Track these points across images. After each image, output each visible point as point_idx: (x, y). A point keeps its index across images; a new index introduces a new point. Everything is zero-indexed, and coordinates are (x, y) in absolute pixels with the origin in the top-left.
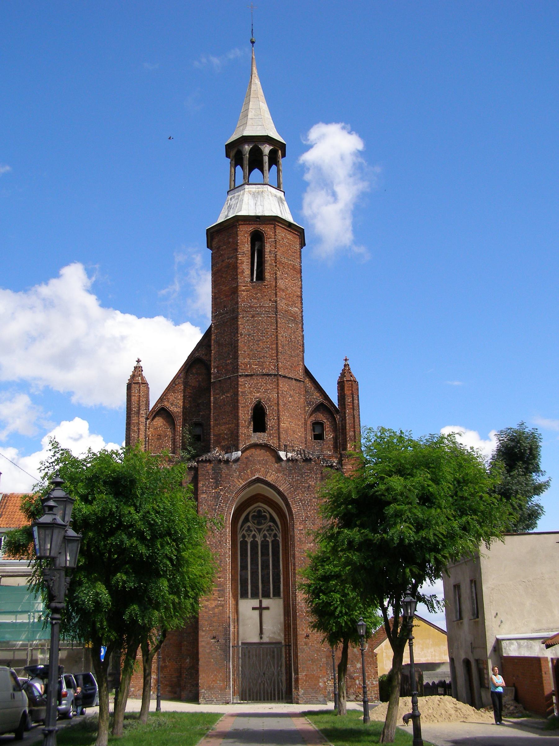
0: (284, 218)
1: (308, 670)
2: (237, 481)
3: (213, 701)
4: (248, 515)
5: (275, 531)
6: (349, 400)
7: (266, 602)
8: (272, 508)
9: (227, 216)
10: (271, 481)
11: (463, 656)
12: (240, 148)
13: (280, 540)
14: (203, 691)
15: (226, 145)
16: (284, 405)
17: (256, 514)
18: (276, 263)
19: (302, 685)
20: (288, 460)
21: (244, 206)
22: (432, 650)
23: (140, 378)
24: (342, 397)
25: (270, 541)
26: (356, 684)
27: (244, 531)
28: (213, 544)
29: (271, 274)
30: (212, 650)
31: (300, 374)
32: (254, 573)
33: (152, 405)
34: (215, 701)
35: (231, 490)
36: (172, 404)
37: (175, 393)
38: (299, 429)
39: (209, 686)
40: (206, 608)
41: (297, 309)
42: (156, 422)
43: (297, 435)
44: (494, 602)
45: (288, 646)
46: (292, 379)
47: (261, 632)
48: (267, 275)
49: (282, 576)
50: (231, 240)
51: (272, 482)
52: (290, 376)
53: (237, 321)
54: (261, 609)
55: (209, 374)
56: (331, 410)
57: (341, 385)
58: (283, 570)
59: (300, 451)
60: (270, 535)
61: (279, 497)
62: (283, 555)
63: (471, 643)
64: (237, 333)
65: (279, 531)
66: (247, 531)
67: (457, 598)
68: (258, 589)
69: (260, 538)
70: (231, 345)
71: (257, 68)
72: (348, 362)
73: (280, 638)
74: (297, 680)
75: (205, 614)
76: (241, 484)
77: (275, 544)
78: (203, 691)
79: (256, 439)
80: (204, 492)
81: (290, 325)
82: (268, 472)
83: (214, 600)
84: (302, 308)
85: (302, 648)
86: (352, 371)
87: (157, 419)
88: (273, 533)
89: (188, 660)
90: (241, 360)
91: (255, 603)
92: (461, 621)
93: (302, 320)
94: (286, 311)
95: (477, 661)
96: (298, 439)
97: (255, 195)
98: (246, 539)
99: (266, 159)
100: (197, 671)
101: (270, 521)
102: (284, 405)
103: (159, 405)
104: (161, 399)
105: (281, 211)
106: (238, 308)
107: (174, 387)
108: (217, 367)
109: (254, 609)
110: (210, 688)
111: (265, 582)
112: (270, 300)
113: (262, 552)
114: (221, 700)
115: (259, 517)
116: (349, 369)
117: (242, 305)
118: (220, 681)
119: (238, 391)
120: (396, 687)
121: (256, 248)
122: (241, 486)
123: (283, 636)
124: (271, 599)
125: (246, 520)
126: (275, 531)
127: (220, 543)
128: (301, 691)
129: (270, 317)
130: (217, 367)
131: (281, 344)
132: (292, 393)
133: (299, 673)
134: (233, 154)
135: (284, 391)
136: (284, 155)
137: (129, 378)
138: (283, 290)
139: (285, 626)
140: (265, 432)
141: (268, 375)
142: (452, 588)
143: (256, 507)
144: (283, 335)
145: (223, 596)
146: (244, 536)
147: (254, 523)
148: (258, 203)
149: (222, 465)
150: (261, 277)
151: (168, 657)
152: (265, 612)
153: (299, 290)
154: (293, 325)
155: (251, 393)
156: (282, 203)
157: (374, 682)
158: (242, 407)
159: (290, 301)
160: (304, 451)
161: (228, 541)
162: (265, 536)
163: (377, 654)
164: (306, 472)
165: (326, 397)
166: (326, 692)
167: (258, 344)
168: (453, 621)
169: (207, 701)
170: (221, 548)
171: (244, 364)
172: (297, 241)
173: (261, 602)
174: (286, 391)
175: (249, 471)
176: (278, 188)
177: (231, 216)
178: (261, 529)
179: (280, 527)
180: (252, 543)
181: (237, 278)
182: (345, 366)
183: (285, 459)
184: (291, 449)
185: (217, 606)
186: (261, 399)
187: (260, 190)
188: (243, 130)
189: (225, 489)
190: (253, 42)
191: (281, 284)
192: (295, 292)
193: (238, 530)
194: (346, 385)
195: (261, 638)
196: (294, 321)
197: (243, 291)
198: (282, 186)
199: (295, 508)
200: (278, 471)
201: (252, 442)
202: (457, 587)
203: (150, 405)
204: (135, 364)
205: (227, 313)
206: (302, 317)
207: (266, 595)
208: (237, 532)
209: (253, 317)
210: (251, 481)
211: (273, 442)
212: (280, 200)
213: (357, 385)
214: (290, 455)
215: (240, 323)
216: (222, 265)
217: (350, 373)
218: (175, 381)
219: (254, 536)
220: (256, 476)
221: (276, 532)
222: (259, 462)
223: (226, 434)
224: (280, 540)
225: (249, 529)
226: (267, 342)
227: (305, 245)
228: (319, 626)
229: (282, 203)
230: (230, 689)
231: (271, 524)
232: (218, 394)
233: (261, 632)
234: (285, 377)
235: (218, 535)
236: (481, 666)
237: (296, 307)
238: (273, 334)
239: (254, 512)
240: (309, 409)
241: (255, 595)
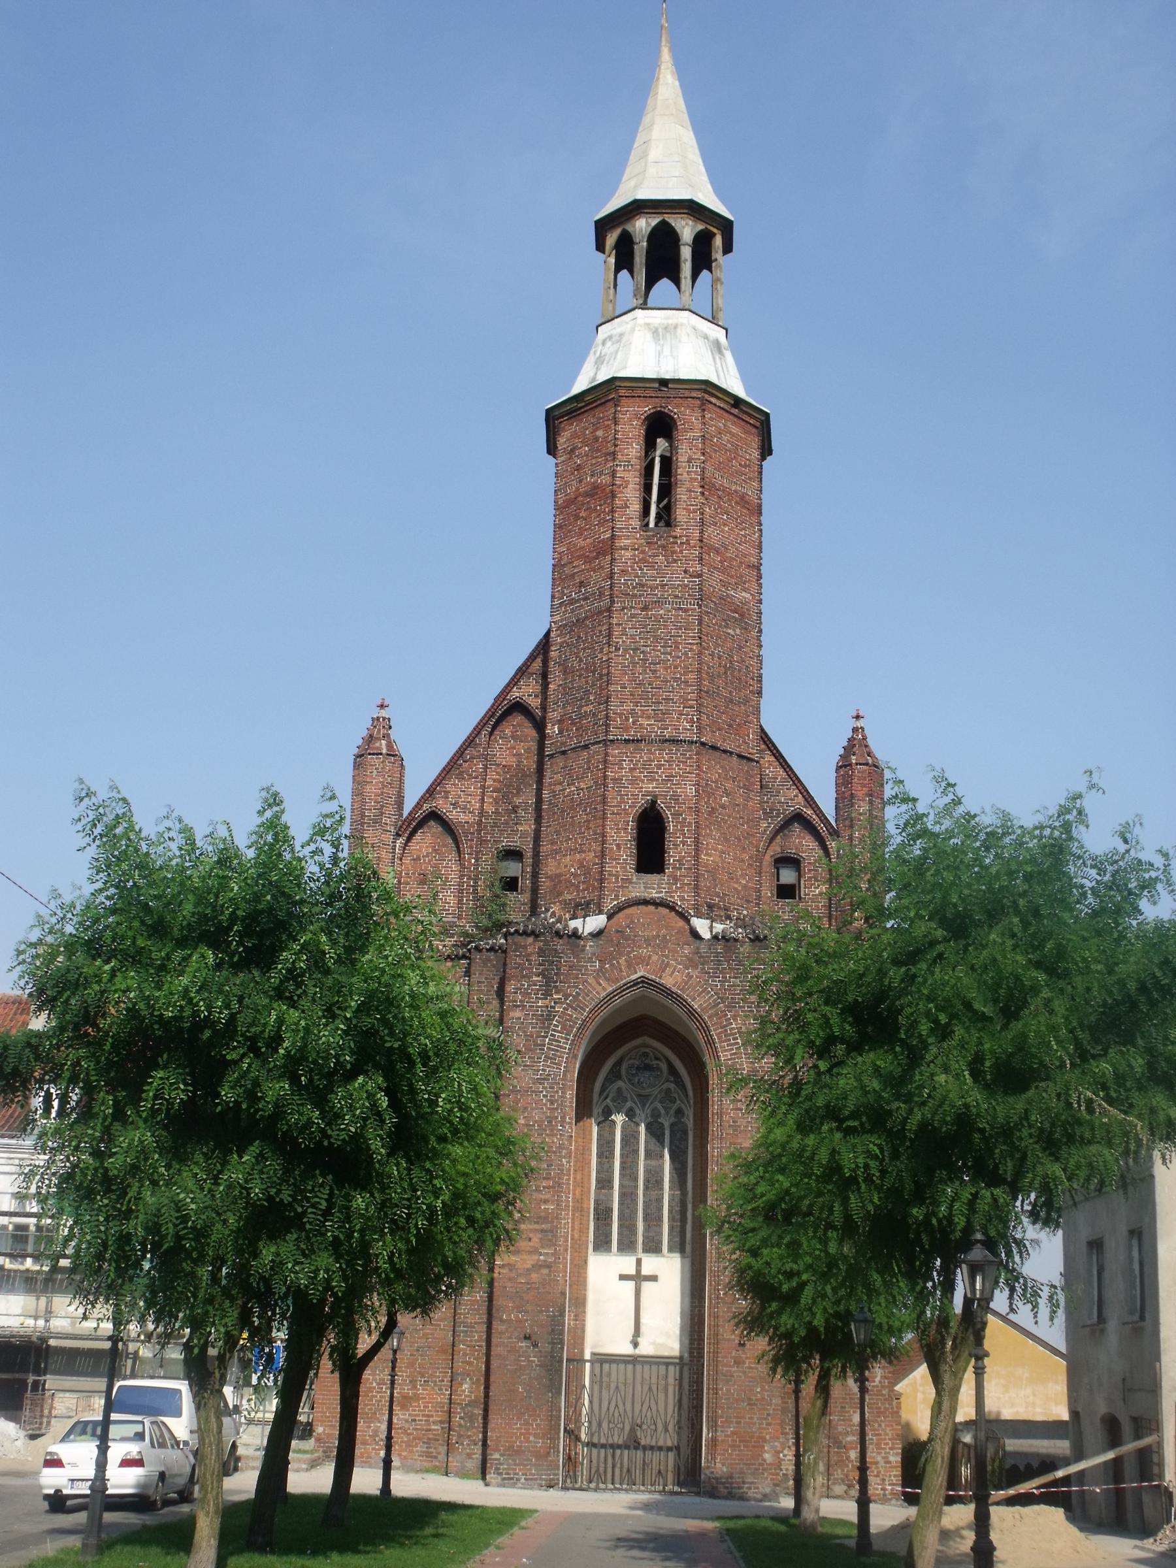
0: (724, 386)
1: (738, 1423)
2: (594, 983)
4: (619, 1063)
7: (651, 1264)
8: (673, 1051)
9: (594, 379)
10: (674, 986)
11: (1102, 1409)
12: (629, 228)
14: (496, 1456)
15: (596, 222)
18: (702, 487)
19: (723, 1455)
20: (715, 937)
22: (1029, 1391)
23: (383, 742)
24: (844, 800)
25: (667, 1124)
26: (848, 1458)
27: (608, 1100)
28: (534, 1125)
29: (689, 511)
30: (521, 1366)
31: (752, 746)
32: (628, 1196)
33: (408, 807)
34: (523, 1480)
35: (581, 1001)
36: (455, 805)
37: (464, 778)
38: (742, 869)
39: (511, 1447)
40: (511, 1270)
41: (747, 595)
42: (417, 843)
43: (737, 882)
46: (731, 753)
48: (680, 514)
50: (600, 433)
51: (674, 989)
54: (638, 1278)
55: (542, 736)
56: (818, 831)
57: (844, 766)
58: (693, 1193)
62: (694, 1157)
63: (1124, 1379)
65: (689, 1102)
67: (1095, 1272)
69: (643, 1116)
70: (593, 672)
71: (672, 50)
74: (714, 1442)
75: (509, 1285)
76: (604, 989)
78: (496, 1456)
79: (642, 889)
80: (519, 1006)
81: (730, 631)
82: (668, 965)
83: (530, 1253)
85: (727, 1371)
86: (870, 741)
87: (418, 836)
88: (675, 1107)
89: (465, 1386)
90: (614, 706)
91: (627, 1264)
92: (1101, 1326)
96: (738, 892)
97: (656, 333)
99: (686, 253)
103: (426, 806)
104: (431, 793)
105: (717, 372)
107: (461, 765)
108: (558, 721)
109: (623, 1277)
110: (513, 1452)
112: (685, 572)
113: (647, 1151)
114: (536, 1479)
116: (865, 738)
118: (536, 1436)
121: (658, 453)
122: (604, 994)
124: (663, 1256)
125: (615, 1074)
129: (686, 611)
130: (560, 722)
131: (708, 673)
133: (719, 1429)
134: (611, 239)
135: (712, 782)
136: (728, 248)
138: (717, 552)
139: (692, 1319)
140: (664, 873)
141: (674, 741)
142: (1084, 1248)
143: (637, 1047)
145: (552, 1243)
148: (667, 351)
149: (560, 944)
150: (666, 517)
151: (423, 1376)
152: (646, 1286)
154: (738, 631)
155: (634, 781)
156: (720, 352)
157: (892, 1459)
158: (613, 813)
159: (732, 577)
161: (568, 1120)
163: (901, 1394)
164: (754, 969)
165: (809, 800)
166: (778, 1474)
167: (654, 672)
168: (1084, 1327)
169: (504, 1479)
170: (553, 1135)
171: (620, 715)
172: (755, 442)
173: (639, 1262)
174: (716, 782)
175: (622, 960)
176: (713, 320)
177: (602, 377)
178: (647, 1096)
179: (691, 1093)
182: (855, 730)
184: (722, 914)
185: (537, 1267)
186: (656, 796)
187: (670, 322)
188: (636, 187)
189: (566, 999)
192: (745, 556)
195: (635, 1344)
198: (721, 315)
199: (726, 1051)
200: (691, 963)
201: (633, 895)
202: (1096, 1245)
203: (405, 806)
205: (585, 599)
207: (653, 1247)
208: (591, 1101)
209: (645, 608)
211: (682, 897)
212: (717, 345)
214: (719, 927)
216: (578, 489)
217: (866, 746)
218: (463, 753)
221: (683, 1106)
222: (648, 941)
223: (575, 875)
226: (676, 667)
228: (754, 1323)
229: (720, 352)
230: (558, 1456)
232: (561, 784)
235: (545, 1105)
237: (745, 590)
238: (691, 650)
240: (766, 826)
241: (627, 1246)
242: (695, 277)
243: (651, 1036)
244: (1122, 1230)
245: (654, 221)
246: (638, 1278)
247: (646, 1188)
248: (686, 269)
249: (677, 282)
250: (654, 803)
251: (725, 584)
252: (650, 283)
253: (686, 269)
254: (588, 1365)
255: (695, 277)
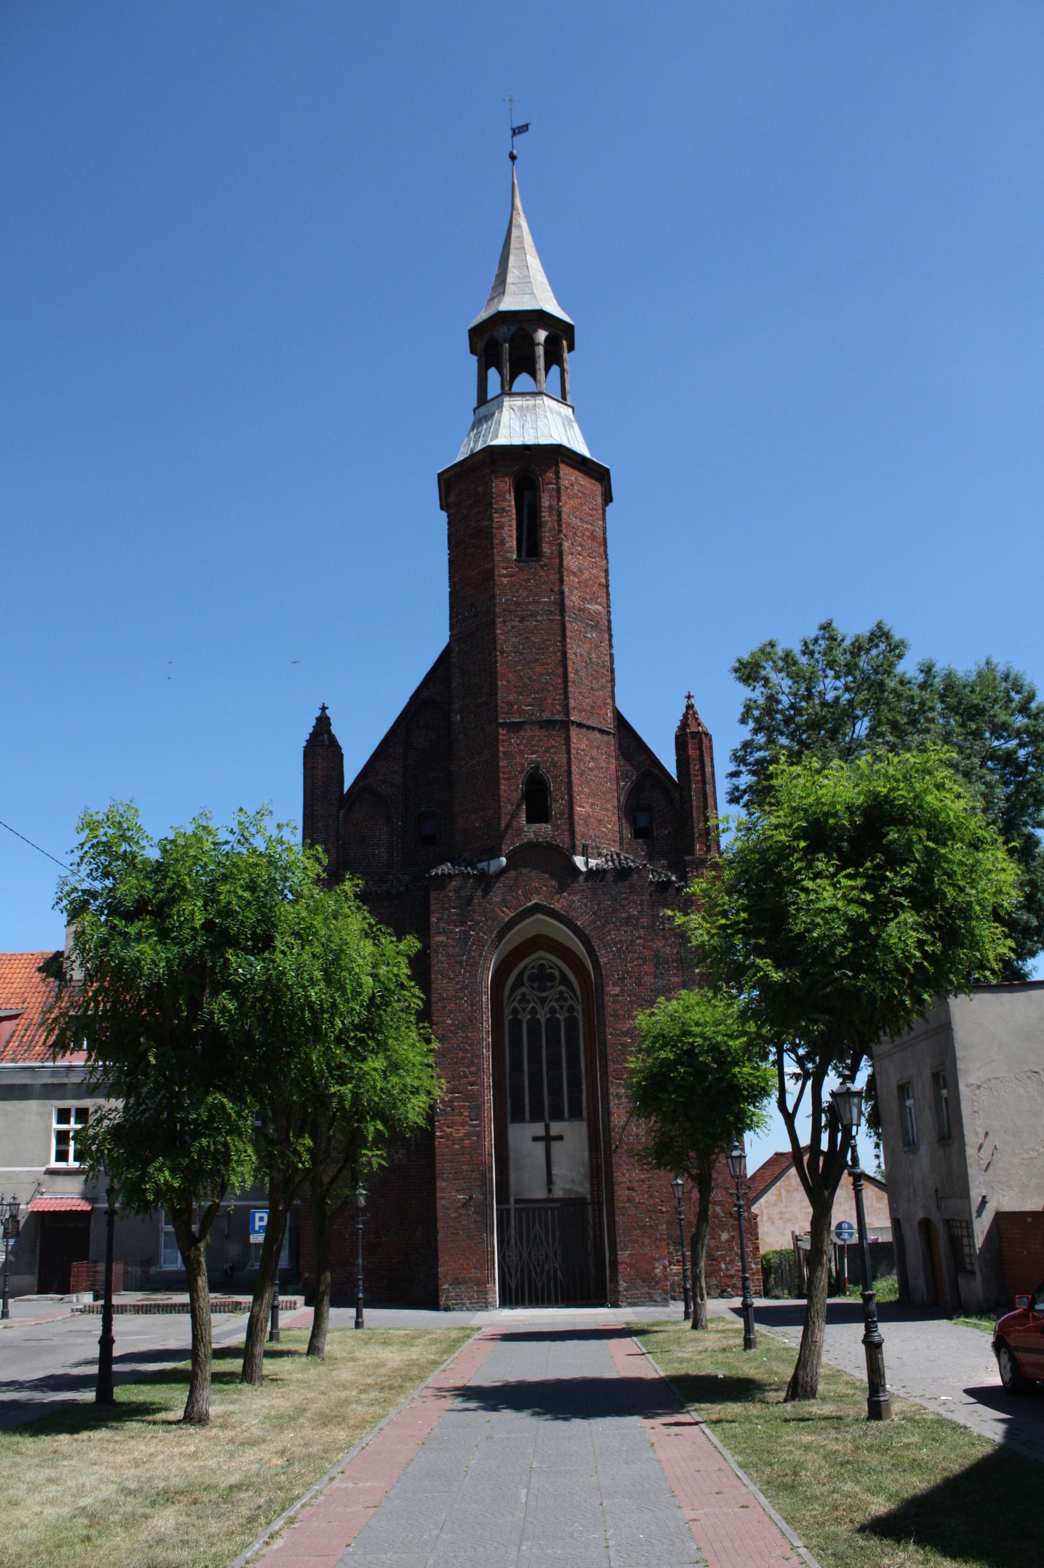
3: (464, 1304)
4: (521, 973)
5: (570, 1002)
6: (695, 767)
7: (556, 1128)
11: (920, 1215)
13: (580, 1017)
14: (446, 1286)
16: (581, 775)
17: (535, 971)
21: (503, 431)
26: (720, 1269)
31: (609, 724)
41: (600, 608)
44: (981, 1112)
45: (597, 1203)
47: (550, 1180)
49: (584, 1081)
50: (480, 489)
51: (562, 912)
52: (590, 723)
53: (495, 629)
54: (548, 1139)
59: (612, 856)
60: (562, 1008)
61: (576, 939)
63: (936, 1191)
64: (495, 648)
66: (520, 1002)
68: (542, 1103)
72: (693, 701)
73: (584, 1189)
74: (614, 1264)
76: (507, 915)
77: (572, 1023)
78: (446, 1286)
83: (463, 1124)
84: (609, 606)
91: (538, 1129)
93: (610, 629)
94: (580, 610)
95: (948, 1223)
96: (606, 834)
98: (519, 1017)
99: (540, 351)
100: (435, 1251)
101: (561, 984)
102: (581, 775)
103: (361, 784)
106: (495, 606)
109: (536, 1139)
111: (555, 1091)
115: (542, 977)
117: (502, 599)
119: (498, 751)
120: (324, 1293)
121: (526, 502)
123: (588, 1186)
125: (519, 982)
126: (570, 1002)
127: (471, 1021)
128: (623, 1285)
132: (594, 753)
134: (481, 345)
136: (571, 348)
137: (308, 737)
138: (574, 574)
144: (575, 650)
146: (515, 1012)
147: (532, 987)
148: (527, 426)
152: (555, 1145)
153: (603, 574)
154: (594, 635)
160: (618, 855)
162: (552, 1011)
172: (597, 488)
173: (547, 1128)
174: (584, 750)
176: (563, 398)
180: (529, 1023)
181: (493, 554)
183: (583, 869)
185: (468, 1135)
188: (499, 302)
190: (513, 157)
191: (571, 561)
192: (597, 577)
193: (505, 1000)
194: (691, 745)
195: (550, 1191)
196: (596, 627)
197: (505, 576)
198: (568, 397)
204: (318, 713)
206: (609, 621)
210: (524, 910)
213: (711, 740)
214: (593, 863)
215: (499, 632)
219: (533, 1011)
220: (534, 902)
224: (580, 1017)
225: (524, 999)
227: (611, 500)
231: (563, 988)
233: (550, 1180)
234: (580, 725)
236: (957, 1232)
237: (597, 603)
239: (533, 968)
241: (536, 1116)
242: (547, 369)
243: (545, 950)
244: (927, 1073)
245: (513, 328)
246: (548, 1139)
247: (549, 1069)
248: (541, 363)
249: (533, 375)
250: (537, 768)
251: (584, 600)
252: (513, 377)
253: (541, 363)
254: (590, 1208)
255: (547, 369)
